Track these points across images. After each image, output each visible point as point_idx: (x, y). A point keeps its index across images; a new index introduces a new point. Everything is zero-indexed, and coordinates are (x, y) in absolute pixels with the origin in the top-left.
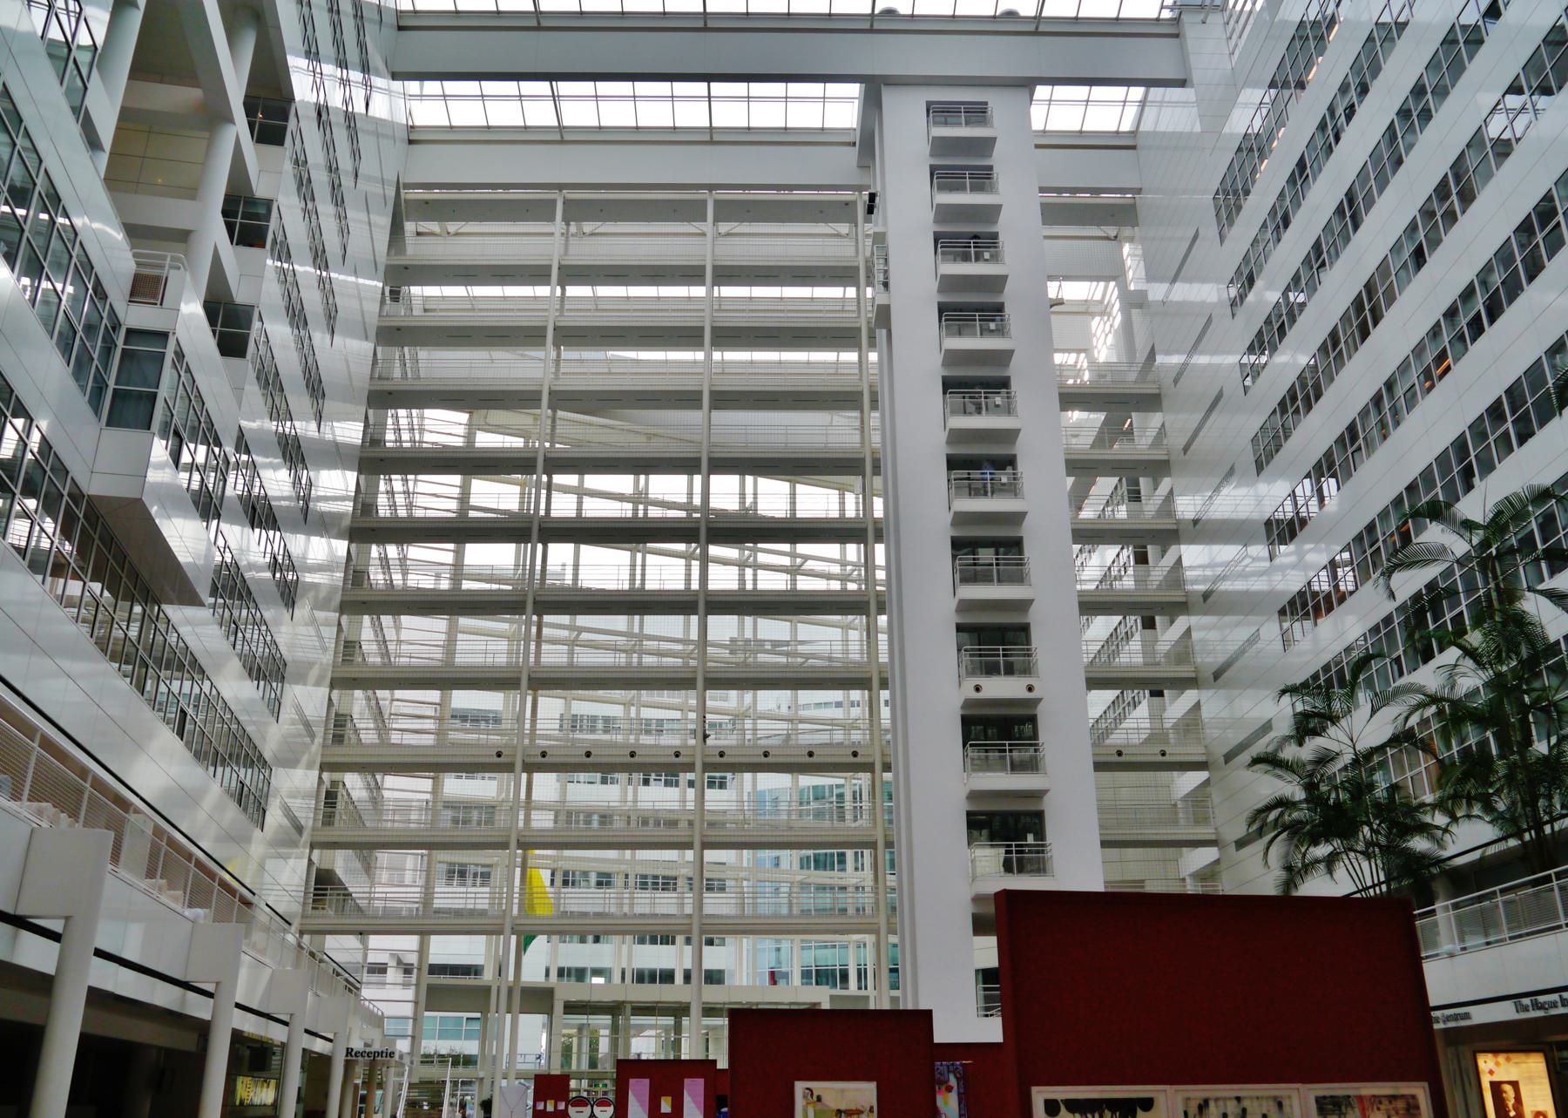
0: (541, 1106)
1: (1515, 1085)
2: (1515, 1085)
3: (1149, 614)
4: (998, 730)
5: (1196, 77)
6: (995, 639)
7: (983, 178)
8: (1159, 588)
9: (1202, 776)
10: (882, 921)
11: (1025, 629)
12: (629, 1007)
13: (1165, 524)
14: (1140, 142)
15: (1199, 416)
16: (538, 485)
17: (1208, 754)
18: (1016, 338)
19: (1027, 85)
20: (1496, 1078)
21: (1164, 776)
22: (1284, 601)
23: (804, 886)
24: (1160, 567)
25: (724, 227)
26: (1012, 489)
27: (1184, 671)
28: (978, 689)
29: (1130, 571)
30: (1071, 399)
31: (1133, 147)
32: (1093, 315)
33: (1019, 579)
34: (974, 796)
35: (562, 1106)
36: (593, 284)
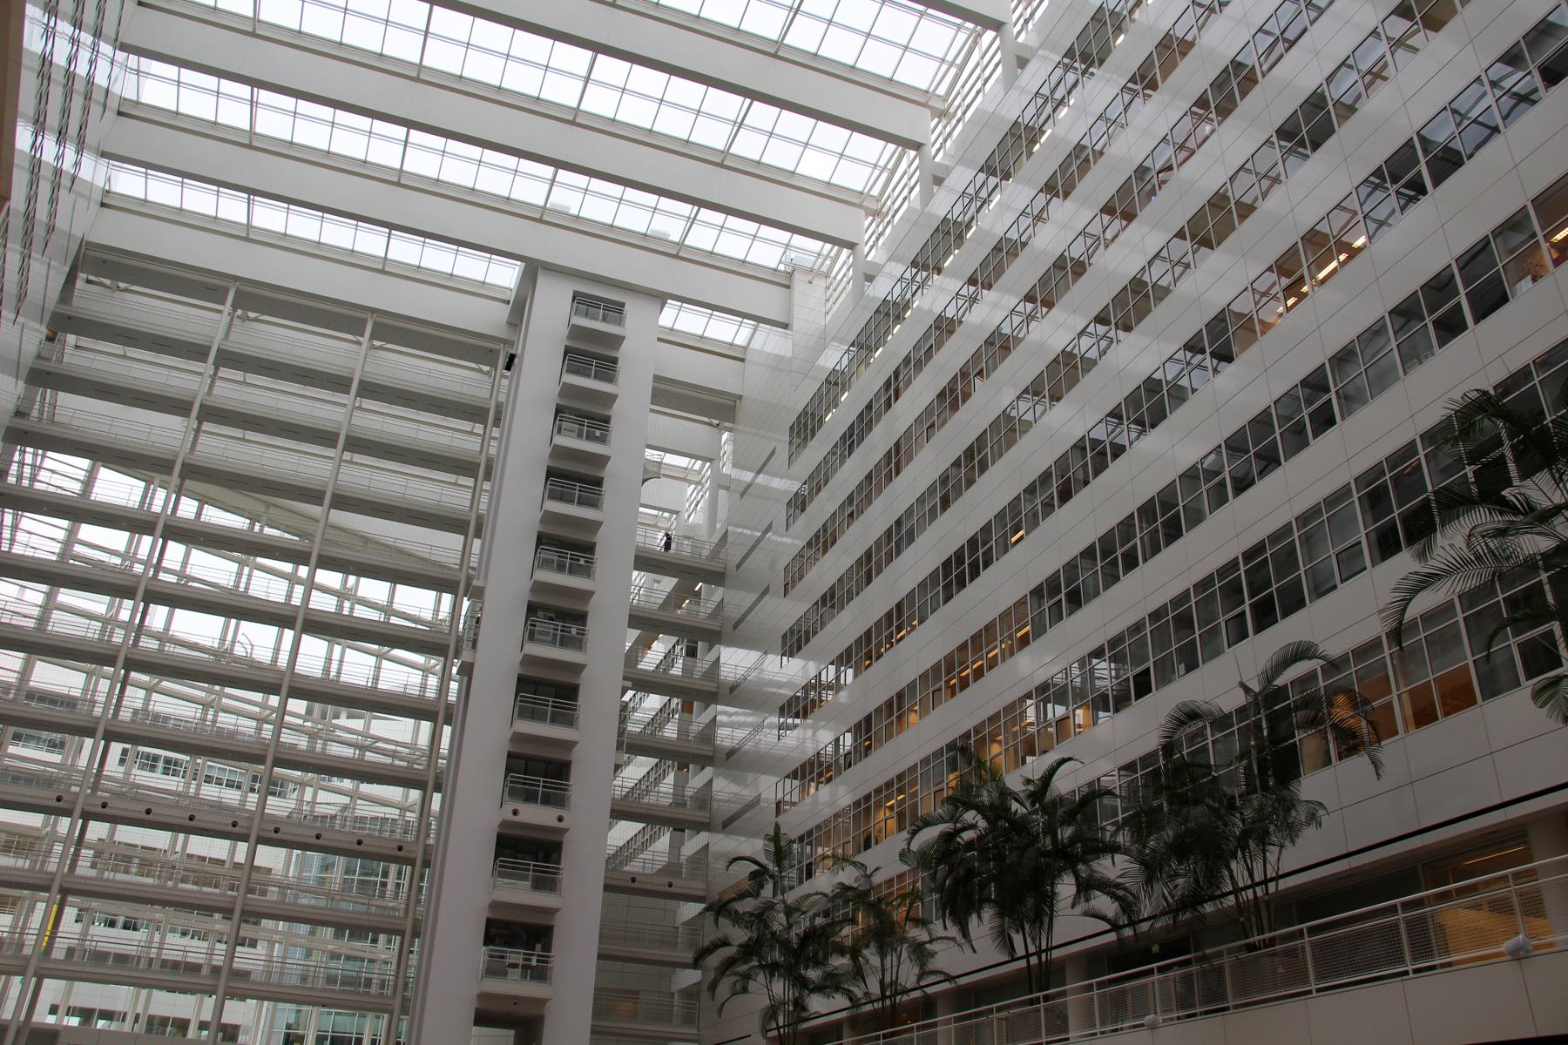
5: (796, 325)
7: (607, 367)
10: (397, 1003)
13: (710, 686)
14: (748, 357)
16: (113, 679)
18: (609, 512)
22: (797, 765)
23: (335, 956)
25: (347, 456)
27: (701, 816)
28: (515, 812)
30: (645, 562)
31: (742, 360)
32: (690, 482)
33: (570, 722)
36: (246, 371)
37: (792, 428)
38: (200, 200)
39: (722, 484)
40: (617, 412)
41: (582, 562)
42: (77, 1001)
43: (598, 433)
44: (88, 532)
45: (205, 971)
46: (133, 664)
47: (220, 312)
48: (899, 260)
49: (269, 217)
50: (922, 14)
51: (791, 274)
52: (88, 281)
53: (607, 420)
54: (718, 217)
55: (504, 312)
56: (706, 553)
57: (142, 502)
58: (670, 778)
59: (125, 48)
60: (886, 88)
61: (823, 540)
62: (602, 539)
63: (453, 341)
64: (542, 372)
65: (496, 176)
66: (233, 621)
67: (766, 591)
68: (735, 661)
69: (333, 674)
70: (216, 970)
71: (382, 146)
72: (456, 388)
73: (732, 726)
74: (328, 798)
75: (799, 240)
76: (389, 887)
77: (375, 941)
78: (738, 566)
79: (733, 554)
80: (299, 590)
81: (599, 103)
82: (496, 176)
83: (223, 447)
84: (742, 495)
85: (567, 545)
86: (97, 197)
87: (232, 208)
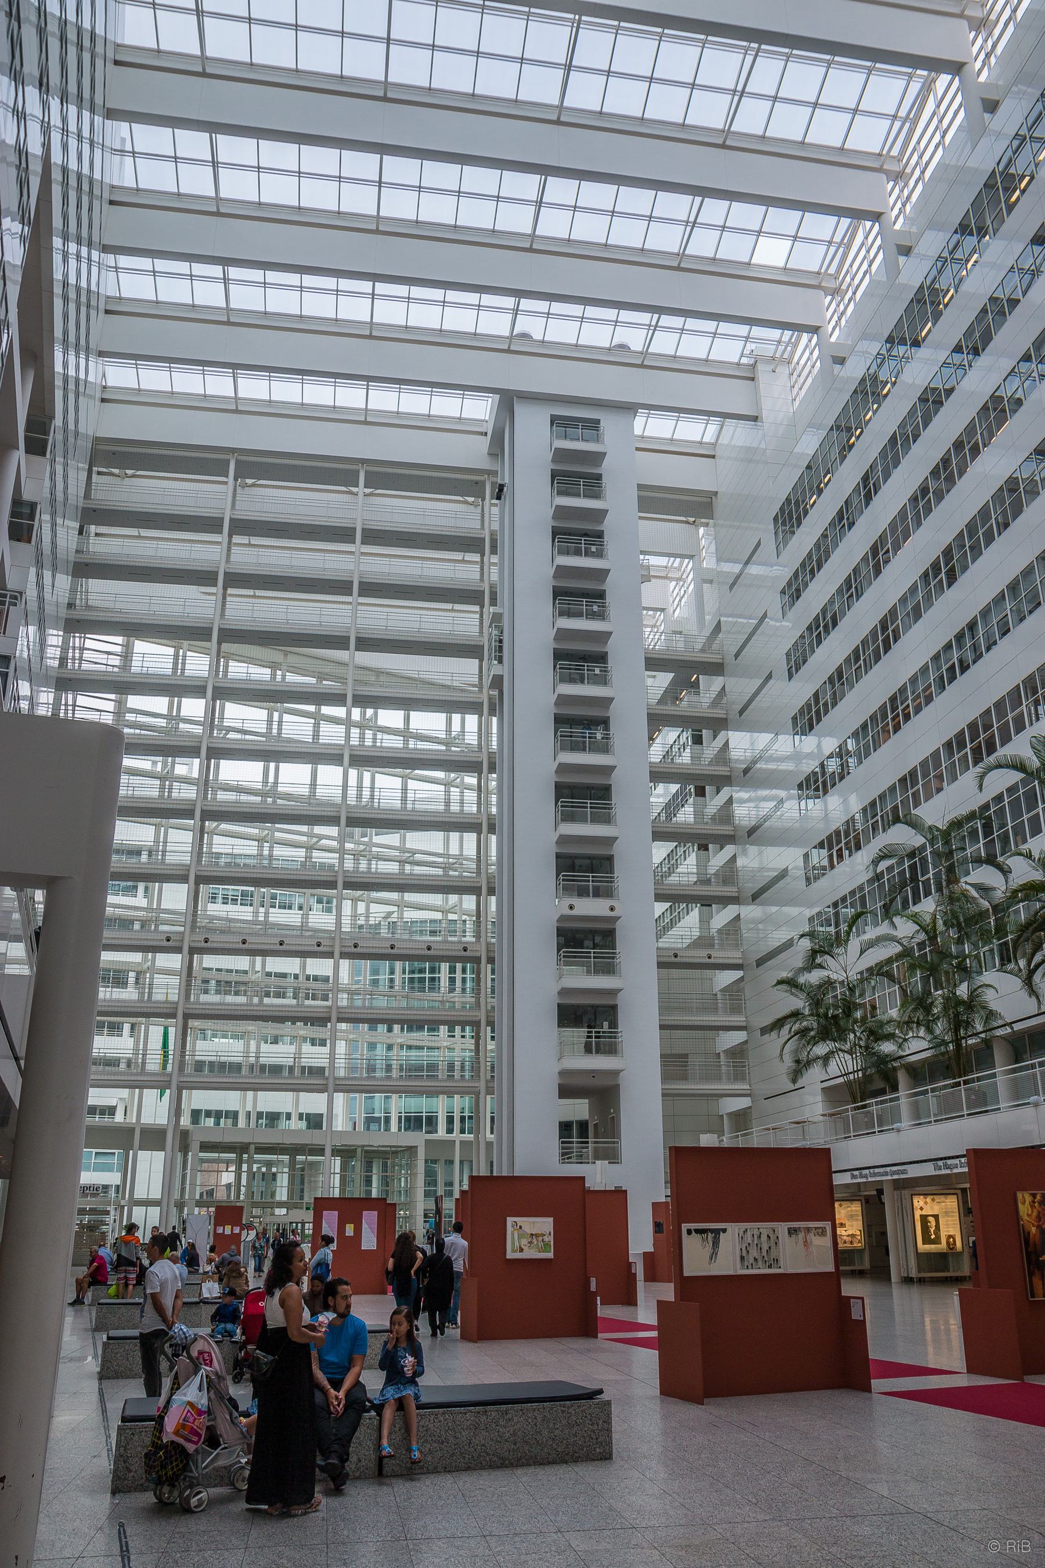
0: (220, 1230)
1: (936, 1217)
2: (936, 1217)
3: (700, 785)
4: (585, 941)
6: (584, 867)
7: (593, 484)
8: (710, 764)
9: (739, 974)
11: (610, 859)
12: (252, 1147)
13: (722, 770)
14: (718, 454)
15: (759, 682)
17: (744, 958)
19: (630, 409)
20: (924, 1213)
21: (708, 973)
24: (711, 748)
25: (362, 600)
26: (605, 748)
27: (729, 891)
28: (571, 907)
29: (688, 750)
30: (654, 663)
31: (713, 457)
32: (671, 579)
34: (564, 992)
35: (237, 1230)
37: (776, 519)
38: (188, 382)
39: (704, 579)
40: (608, 525)
41: (597, 671)
42: (304, 1109)
43: (593, 549)
44: (134, 701)
45: (244, 1071)
46: (208, 815)
47: (226, 483)
48: (872, 338)
49: (254, 388)
50: (829, 64)
51: (754, 366)
52: (99, 473)
53: (600, 535)
54: (677, 321)
55: (483, 444)
56: (699, 646)
57: (175, 668)
58: (692, 859)
59: (106, 249)
60: (840, 159)
61: (824, 624)
62: (613, 647)
63: (440, 478)
64: (534, 501)
65: (460, 314)
66: (272, 765)
67: (770, 677)
68: (741, 744)
69: (365, 800)
70: (252, 1066)
71: (352, 303)
72: (452, 523)
73: (748, 806)
74: (376, 910)
75: (757, 331)
76: (397, 983)
77: (390, 1030)
78: (737, 656)
79: (728, 642)
80: (355, 732)
81: (554, 225)
82: (460, 314)
83: (248, 608)
84: (731, 587)
85: (580, 658)
86: (98, 395)
87: (219, 385)
